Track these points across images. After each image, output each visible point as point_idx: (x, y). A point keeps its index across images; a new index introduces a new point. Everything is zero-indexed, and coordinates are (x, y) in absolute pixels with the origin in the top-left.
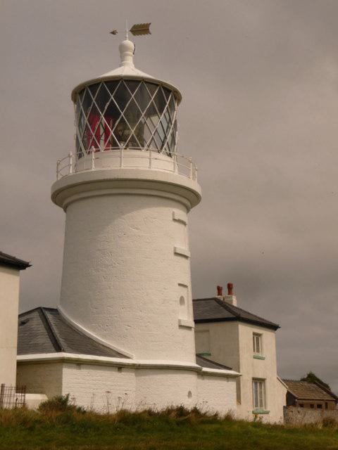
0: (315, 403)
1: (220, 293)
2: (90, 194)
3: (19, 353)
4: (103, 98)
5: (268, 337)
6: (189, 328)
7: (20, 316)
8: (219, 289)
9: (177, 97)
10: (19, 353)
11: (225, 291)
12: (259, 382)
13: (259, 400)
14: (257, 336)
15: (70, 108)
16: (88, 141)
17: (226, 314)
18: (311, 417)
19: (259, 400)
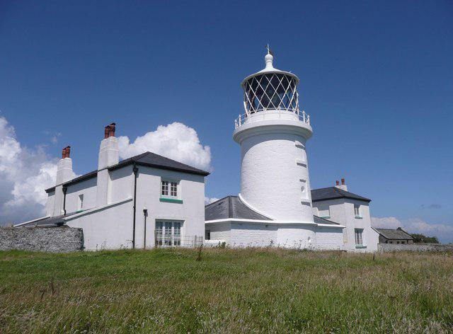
3: (206, 220)
5: (363, 209)
6: (307, 204)
7: (206, 207)
12: (358, 231)
14: (132, 200)
17: (338, 195)
18: (388, 247)
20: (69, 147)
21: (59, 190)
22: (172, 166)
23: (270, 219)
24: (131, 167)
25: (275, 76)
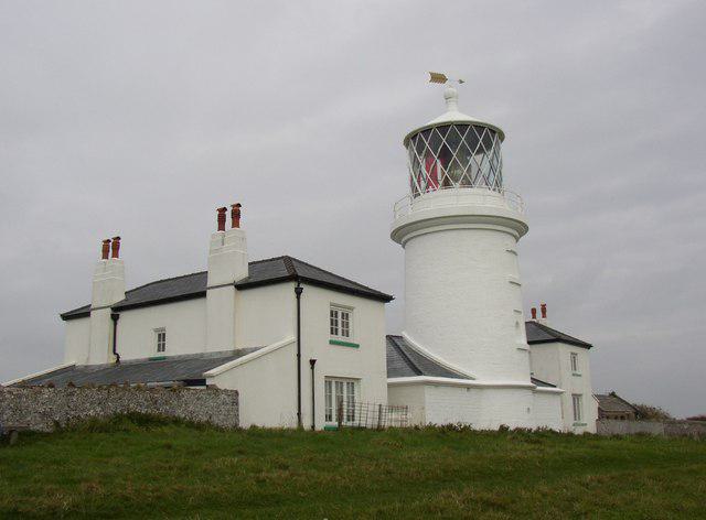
0: (620, 415)
1: (534, 317)
2: (431, 230)
4: (435, 143)
8: (534, 311)
9: (502, 137)
10: (391, 373)
11: (539, 313)
13: (576, 414)
14: (574, 355)
15: (404, 155)
16: (424, 181)
18: (619, 427)
19: (576, 414)
20: (119, 238)
21: (101, 319)
22: (349, 286)
23: (468, 378)
24: (292, 286)
25: (453, 131)
